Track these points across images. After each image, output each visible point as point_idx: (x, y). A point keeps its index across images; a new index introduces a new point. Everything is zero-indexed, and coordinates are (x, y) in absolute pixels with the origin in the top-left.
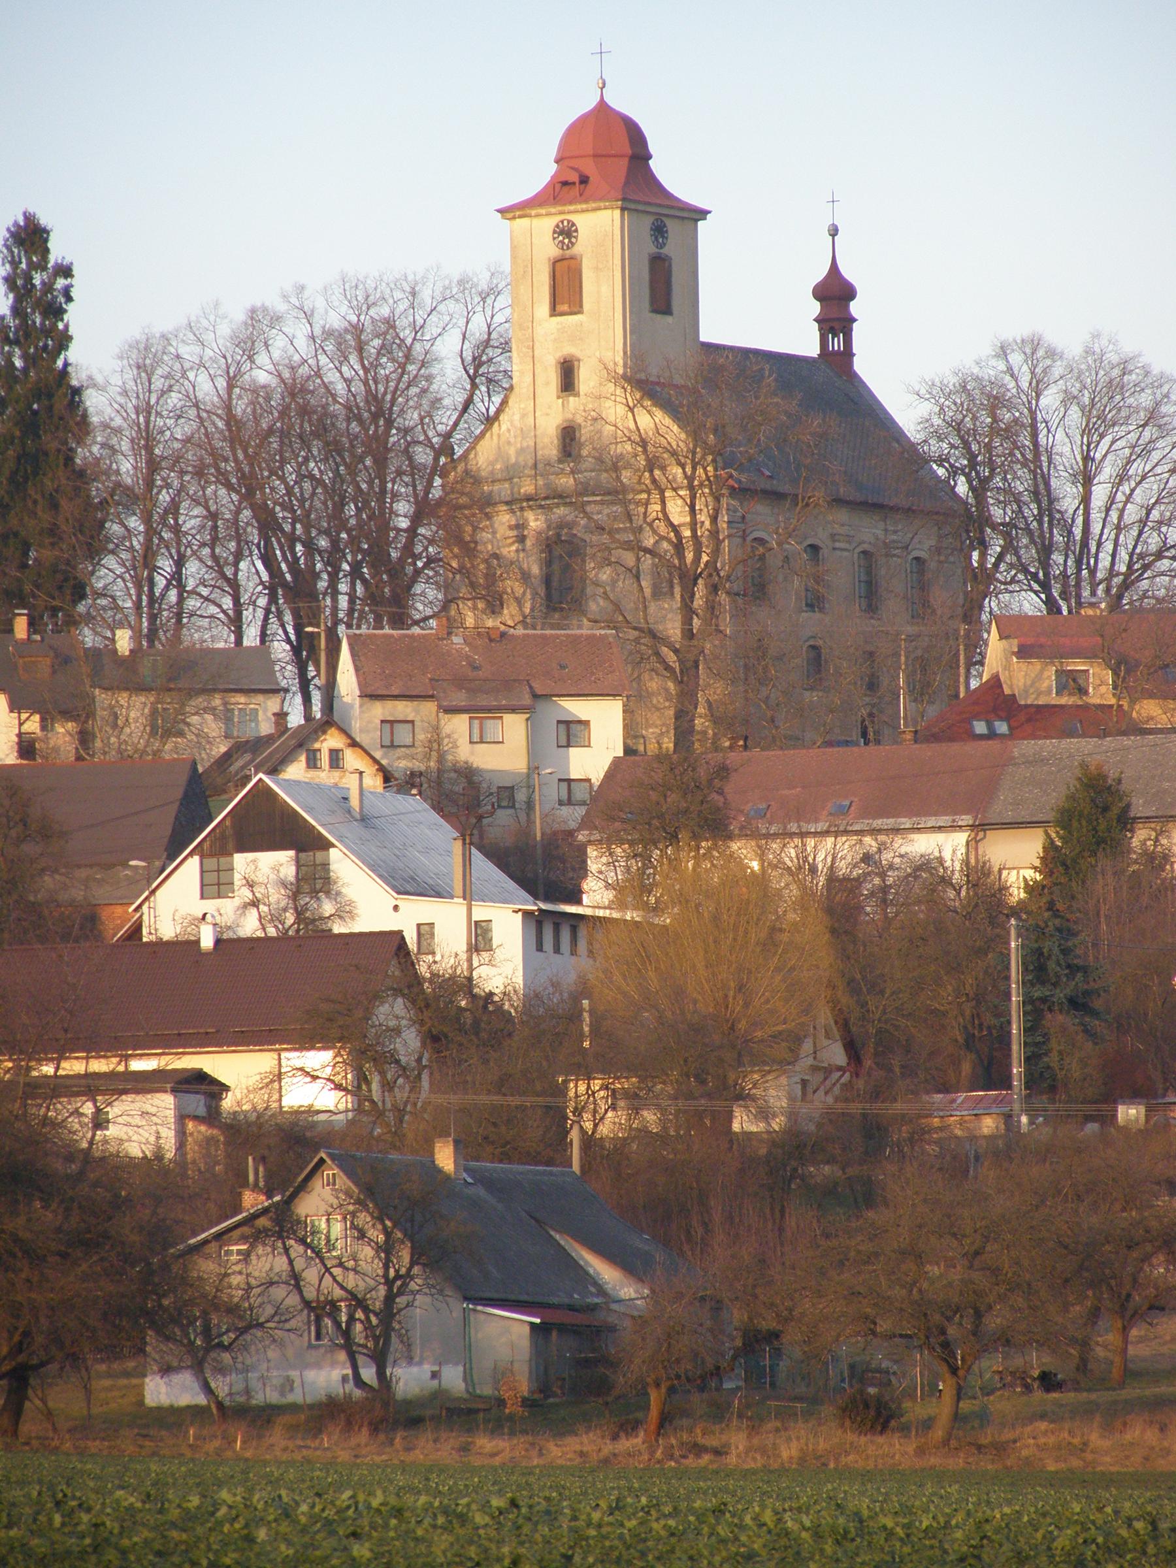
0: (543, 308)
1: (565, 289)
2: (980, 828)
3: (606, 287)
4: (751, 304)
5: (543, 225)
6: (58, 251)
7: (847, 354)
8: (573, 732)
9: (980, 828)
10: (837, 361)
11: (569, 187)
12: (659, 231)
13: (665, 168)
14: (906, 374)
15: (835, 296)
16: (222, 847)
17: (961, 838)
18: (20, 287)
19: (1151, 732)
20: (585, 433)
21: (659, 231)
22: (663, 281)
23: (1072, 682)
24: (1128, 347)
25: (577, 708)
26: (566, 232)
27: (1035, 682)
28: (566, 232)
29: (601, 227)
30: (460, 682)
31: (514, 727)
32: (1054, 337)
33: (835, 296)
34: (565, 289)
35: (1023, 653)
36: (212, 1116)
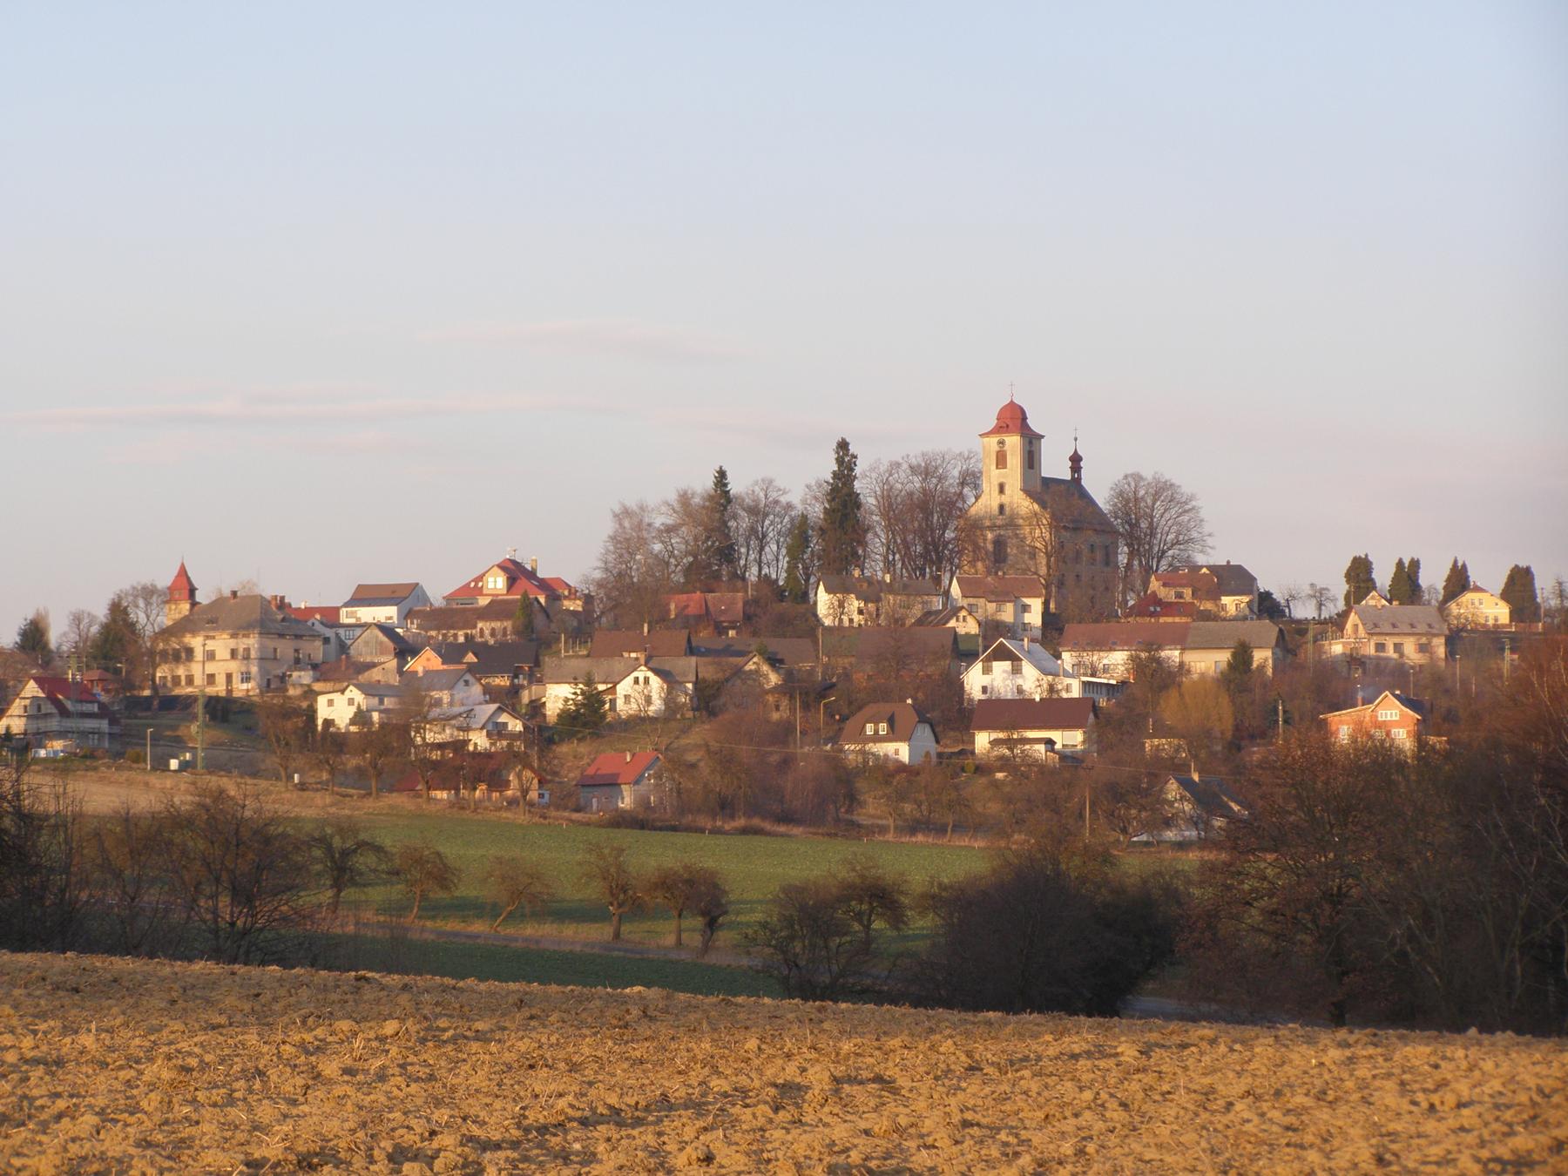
0: (994, 467)
1: (1001, 460)
2: (1183, 649)
3: (1015, 461)
4: (1054, 466)
5: (994, 440)
6: (852, 449)
7: (1079, 479)
8: (1026, 608)
9: (1183, 649)
10: (1076, 481)
11: (1001, 428)
12: (1031, 443)
13: (1032, 423)
14: (1100, 488)
15: (1076, 460)
16: (989, 660)
17: (1177, 653)
18: (840, 461)
19: (1224, 619)
20: (1007, 509)
21: (1031, 443)
22: (1031, 459)
23: (1179, 595)
24: (1167, 477)
25: (1027, 601)
26: (1002, 443)
27: (1167, 594)
28: (1002, 443)
29: (1014, 442)
30: (993, 593)
31: (1009, 607)
32: (1144, 474)
33: (1076, 460)
34: (1001, 460)
35: (1164, 585)
36: (1053, 750)
